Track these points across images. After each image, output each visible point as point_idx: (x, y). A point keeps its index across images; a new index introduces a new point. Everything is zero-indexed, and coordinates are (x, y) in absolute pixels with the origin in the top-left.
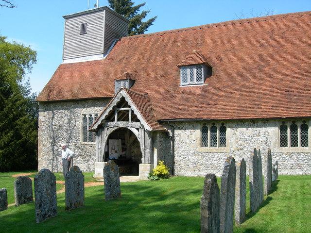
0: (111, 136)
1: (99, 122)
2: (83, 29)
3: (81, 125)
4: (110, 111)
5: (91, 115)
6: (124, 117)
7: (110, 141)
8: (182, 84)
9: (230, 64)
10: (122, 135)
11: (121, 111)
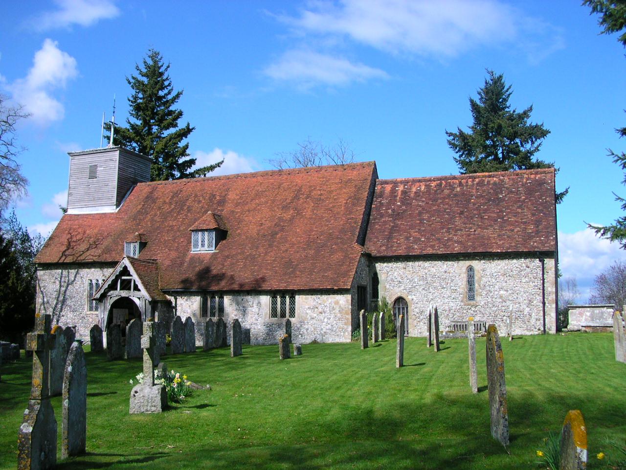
0: (115, 305)
1: (102, 291)
2: (93, 174)
3: (87, 291)
4: (113, 280)
5: (98, 281)
6: (126, 285)
7: (115, 310)
8: (194, 251)
9: (250, 225)
10: (125, 304)
11: (122, 281)
